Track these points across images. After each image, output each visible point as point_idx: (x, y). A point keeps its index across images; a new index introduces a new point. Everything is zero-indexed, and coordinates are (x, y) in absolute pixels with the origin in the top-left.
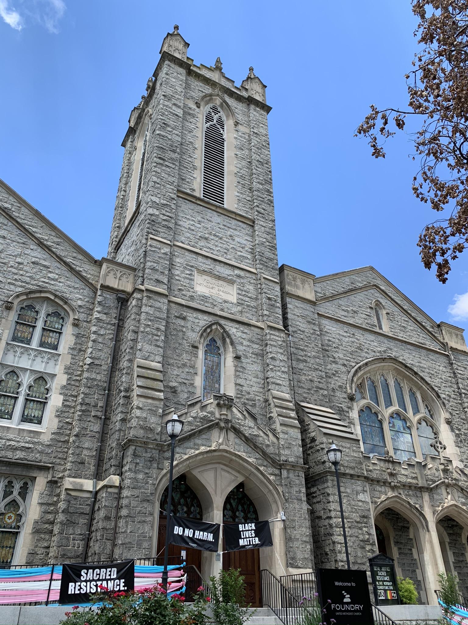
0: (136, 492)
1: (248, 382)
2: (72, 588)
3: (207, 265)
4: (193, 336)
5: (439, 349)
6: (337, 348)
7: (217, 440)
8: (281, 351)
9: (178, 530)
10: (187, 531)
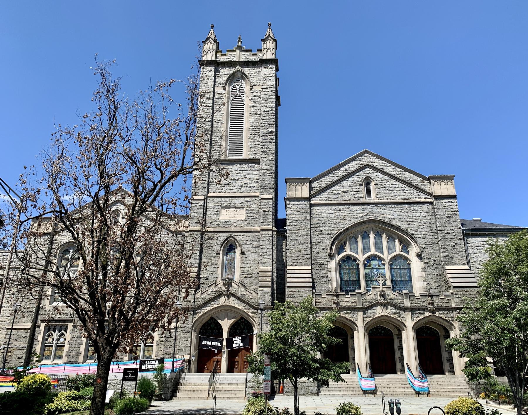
0: (183, 329)
1: (248, 265)
2: (143, 367)
3: (225, 202)
4: (217, 247)
5: (425, 199)
6: (325, 223)
7: (222, 300)
8: (268, 243)
9: (204, 342)
10: (208, 342)
